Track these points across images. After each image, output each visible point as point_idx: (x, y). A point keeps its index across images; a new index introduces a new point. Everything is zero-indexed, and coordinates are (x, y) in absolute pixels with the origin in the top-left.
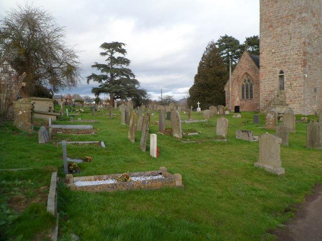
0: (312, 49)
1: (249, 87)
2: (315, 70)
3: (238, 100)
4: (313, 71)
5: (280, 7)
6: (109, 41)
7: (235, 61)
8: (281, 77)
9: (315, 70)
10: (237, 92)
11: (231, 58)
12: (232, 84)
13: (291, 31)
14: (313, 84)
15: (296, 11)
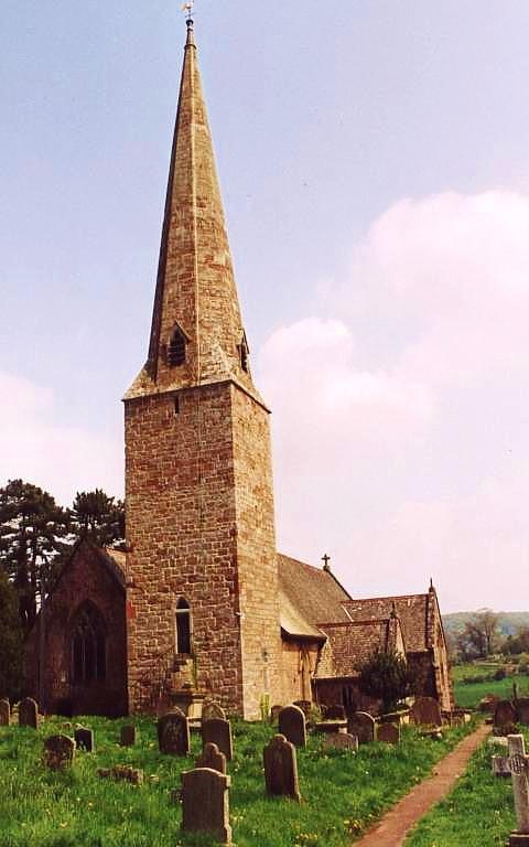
0: (252, 549)
1: (95, 643)
2: (262, 601)
3: (63, 680)
4: (256, 605)
5: (176, 437)
6: (282, 553)
7: (44, 557)
8: (183, 621)
9: (262, 601)
10: (61, 656)
11: (33, 545)
12: (47, 632)
13: (203, 502)
14: (258, 638)
15: (214, 453)
